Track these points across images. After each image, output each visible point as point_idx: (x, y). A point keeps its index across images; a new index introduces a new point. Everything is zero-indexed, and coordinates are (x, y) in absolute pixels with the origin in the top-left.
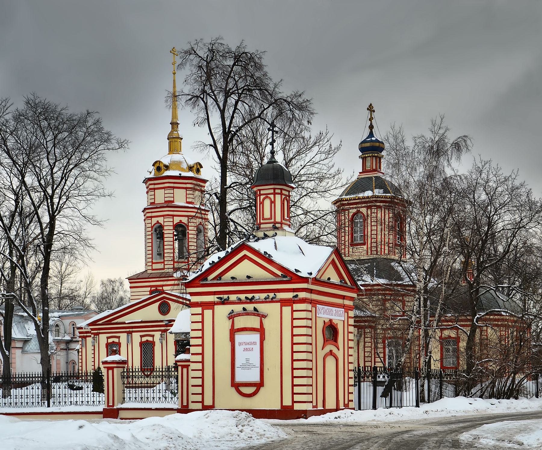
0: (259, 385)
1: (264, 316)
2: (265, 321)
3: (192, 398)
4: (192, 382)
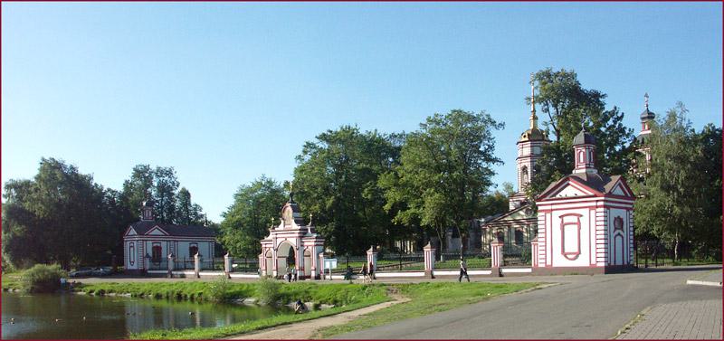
0: (579, 253)
1: (581, 216)
2: (581, 219)
3: (540, 261)
4: (540, 257)
